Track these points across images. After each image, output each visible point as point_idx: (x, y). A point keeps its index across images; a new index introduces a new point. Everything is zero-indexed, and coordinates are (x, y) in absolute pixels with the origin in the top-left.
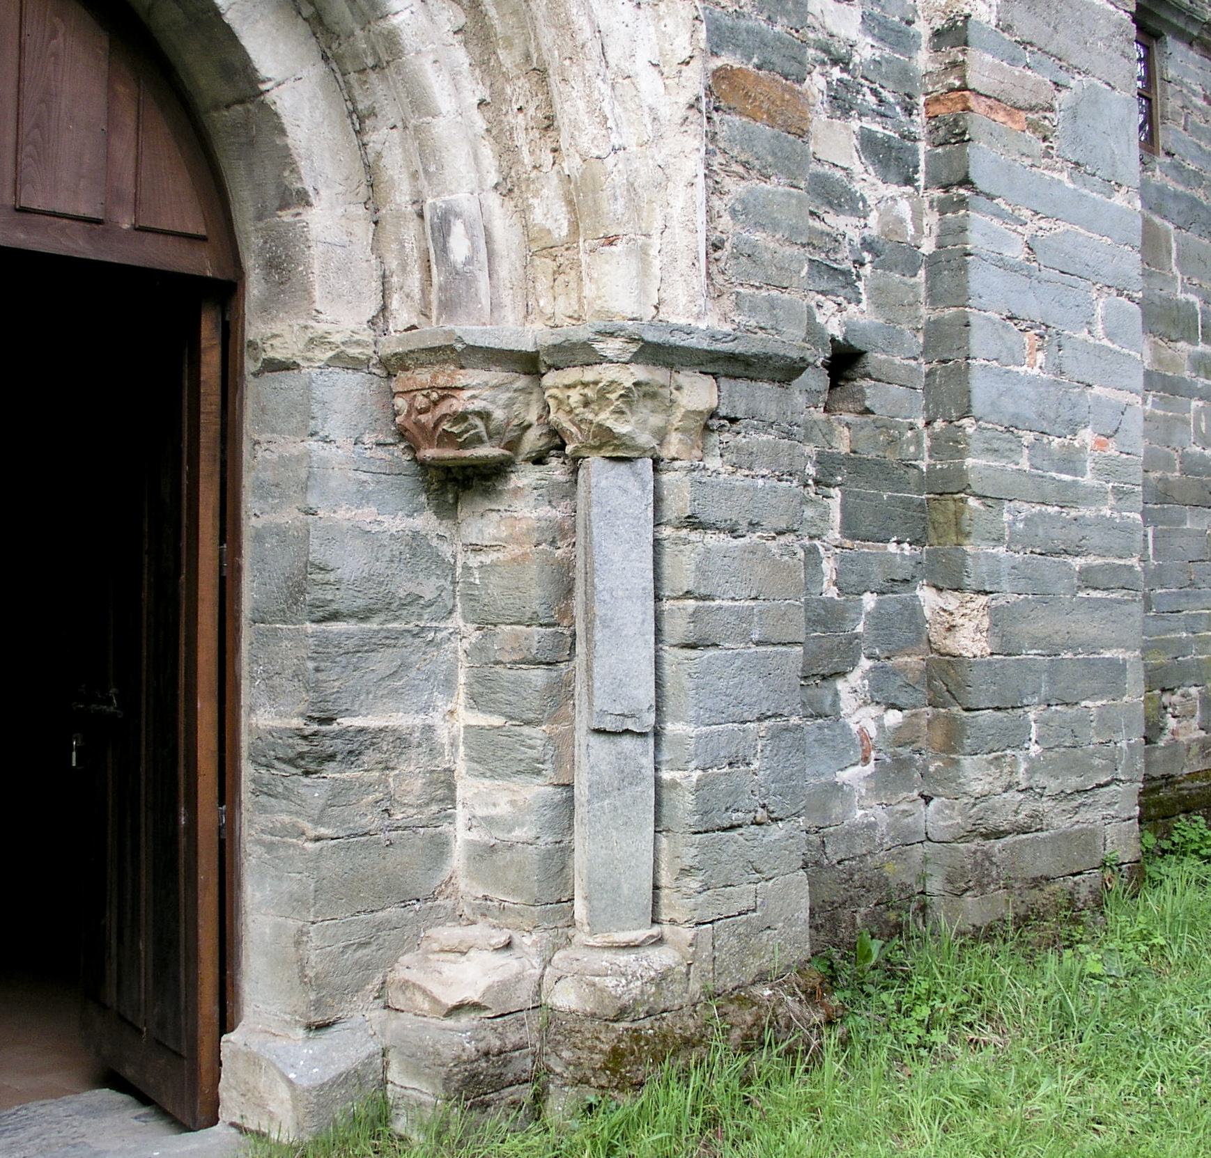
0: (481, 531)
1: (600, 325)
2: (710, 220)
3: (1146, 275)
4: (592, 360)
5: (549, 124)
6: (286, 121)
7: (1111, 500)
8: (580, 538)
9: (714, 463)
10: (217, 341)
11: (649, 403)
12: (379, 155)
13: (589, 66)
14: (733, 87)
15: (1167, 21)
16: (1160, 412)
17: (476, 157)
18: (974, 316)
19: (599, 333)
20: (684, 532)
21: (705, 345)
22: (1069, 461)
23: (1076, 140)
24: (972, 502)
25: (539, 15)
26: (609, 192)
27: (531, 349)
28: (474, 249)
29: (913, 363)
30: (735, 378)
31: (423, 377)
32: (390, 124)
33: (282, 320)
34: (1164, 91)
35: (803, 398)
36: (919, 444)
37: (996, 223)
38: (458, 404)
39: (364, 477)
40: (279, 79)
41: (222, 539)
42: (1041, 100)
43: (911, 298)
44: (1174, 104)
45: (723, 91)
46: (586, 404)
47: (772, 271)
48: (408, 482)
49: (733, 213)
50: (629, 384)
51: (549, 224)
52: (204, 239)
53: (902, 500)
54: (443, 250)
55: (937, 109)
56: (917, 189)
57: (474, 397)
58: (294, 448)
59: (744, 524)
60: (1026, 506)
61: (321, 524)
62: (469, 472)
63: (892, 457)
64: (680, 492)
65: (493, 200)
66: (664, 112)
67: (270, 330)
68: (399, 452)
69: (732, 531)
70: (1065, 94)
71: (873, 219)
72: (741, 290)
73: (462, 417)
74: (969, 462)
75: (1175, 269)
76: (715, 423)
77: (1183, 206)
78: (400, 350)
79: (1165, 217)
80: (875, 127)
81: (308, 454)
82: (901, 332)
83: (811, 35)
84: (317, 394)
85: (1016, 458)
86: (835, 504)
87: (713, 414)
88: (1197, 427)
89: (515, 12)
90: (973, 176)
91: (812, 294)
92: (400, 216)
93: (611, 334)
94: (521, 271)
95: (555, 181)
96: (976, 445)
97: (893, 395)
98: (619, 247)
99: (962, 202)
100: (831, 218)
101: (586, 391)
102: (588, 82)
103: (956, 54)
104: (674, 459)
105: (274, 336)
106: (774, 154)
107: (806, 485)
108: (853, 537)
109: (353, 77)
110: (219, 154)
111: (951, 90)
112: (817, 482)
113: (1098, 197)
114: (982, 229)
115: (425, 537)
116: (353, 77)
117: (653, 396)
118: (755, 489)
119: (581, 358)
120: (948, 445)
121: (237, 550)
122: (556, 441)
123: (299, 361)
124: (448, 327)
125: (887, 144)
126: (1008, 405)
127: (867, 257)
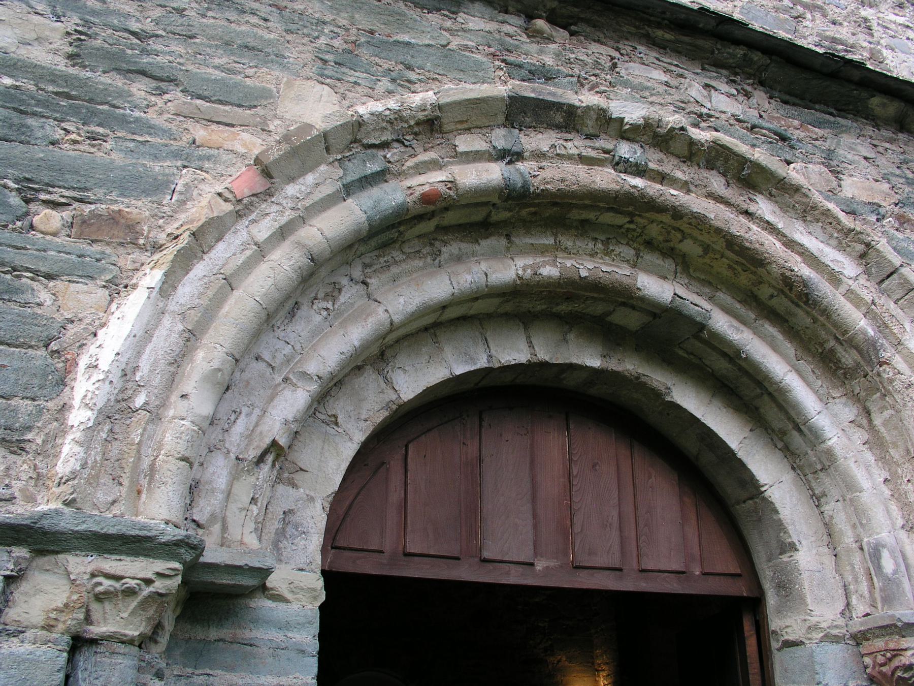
6: (778, 506)
10: (753, 632)
12: (831, 517)
17: (888, 512)
28: (897, 564)
31: (879, 644)
33: (790, 617)
40: (771, 483)
52: (739, 575)
54: (879, 567)
65: (903, 535)
67: (784, 623)
84: (817, 659)
89: (896, 428)
92: (849, 551)
105: (787, 627)
109: (810, 476)
116: (810, 476)
124: (891, 612)
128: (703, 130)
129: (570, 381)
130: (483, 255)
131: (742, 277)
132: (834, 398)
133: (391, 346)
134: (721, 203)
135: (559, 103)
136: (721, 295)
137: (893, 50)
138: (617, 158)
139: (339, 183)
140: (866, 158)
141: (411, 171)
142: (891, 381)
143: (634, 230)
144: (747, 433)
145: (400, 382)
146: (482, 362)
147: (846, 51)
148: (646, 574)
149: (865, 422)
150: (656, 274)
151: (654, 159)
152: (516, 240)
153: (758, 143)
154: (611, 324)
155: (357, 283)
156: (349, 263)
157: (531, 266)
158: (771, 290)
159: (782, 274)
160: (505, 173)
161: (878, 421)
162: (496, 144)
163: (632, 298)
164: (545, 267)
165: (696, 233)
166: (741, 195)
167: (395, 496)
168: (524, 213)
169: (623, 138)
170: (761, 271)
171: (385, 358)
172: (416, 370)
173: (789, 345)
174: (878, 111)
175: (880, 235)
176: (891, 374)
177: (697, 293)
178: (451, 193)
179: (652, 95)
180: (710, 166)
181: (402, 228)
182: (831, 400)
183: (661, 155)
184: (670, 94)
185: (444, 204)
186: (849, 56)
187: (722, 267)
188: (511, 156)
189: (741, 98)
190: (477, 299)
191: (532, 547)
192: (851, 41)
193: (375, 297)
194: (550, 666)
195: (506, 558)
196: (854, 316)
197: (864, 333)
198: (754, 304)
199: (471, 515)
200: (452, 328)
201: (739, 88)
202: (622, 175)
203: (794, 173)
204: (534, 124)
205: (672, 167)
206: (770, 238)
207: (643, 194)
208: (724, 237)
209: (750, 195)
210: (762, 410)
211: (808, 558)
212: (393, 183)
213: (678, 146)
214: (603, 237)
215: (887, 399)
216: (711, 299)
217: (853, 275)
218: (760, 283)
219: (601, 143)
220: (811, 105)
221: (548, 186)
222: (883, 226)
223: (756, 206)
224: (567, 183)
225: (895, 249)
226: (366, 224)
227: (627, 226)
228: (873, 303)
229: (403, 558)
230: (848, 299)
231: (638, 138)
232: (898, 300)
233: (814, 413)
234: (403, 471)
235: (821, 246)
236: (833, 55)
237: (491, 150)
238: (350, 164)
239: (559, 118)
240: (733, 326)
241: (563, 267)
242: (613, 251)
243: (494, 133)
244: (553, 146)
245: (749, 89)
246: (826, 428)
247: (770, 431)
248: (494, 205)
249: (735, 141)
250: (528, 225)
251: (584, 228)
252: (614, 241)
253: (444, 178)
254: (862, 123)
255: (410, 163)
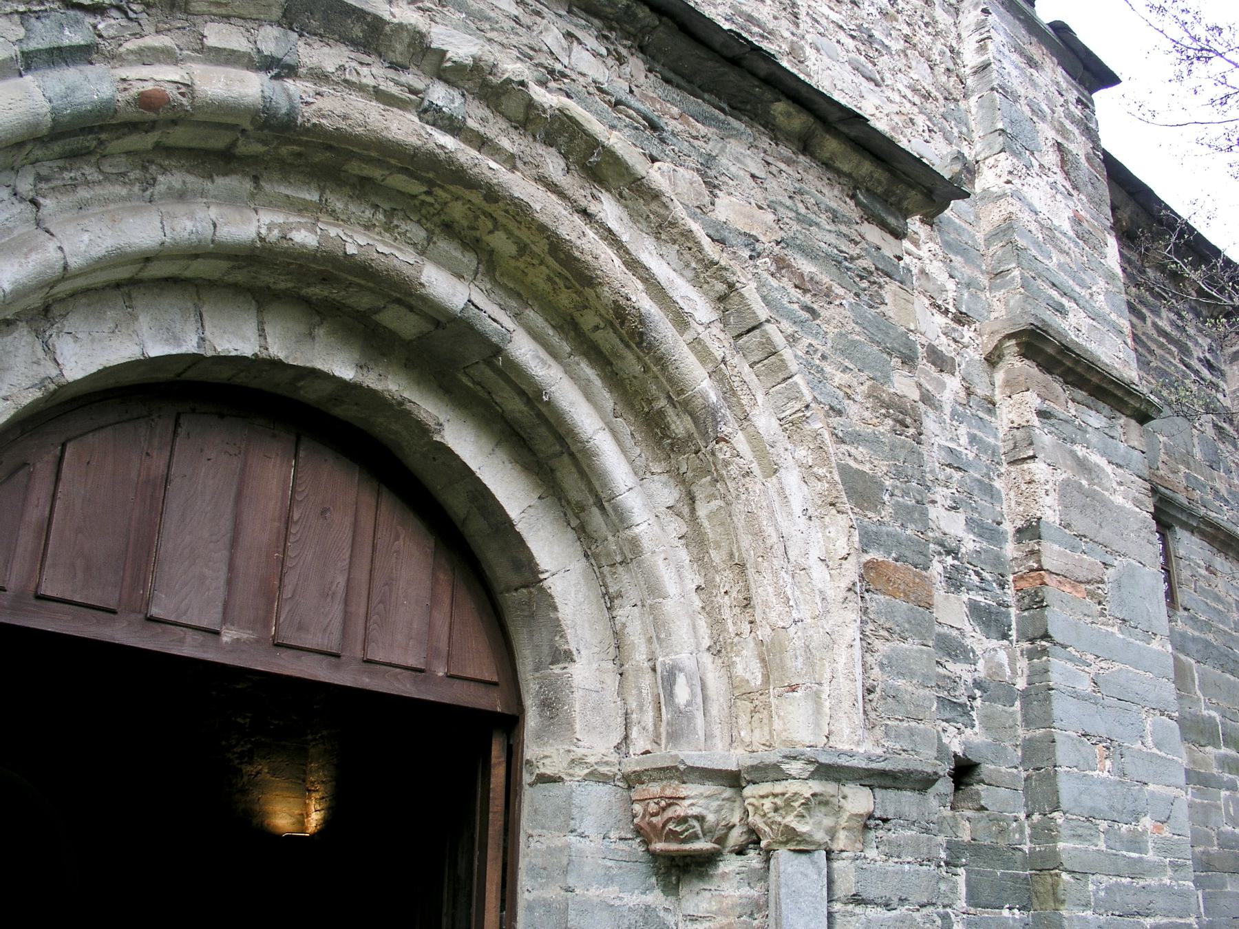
0: (697, 905)
1: (786, 751)
2: (865, 671)
3: (1180, 698)
4: (780, 776)
5: (747, 604)
6: (558, 601)
7: (1170, 872)
8: (772, 911)
9: (872, 853)
10: (503, 759)
11: (823, 809)
12: (624, 625)
13: (775, 562)
14: (879, 575)
15: (1174, 517)
16: (1198, 801)
17: (694, 627)
18: (1058, 735)
19: (785, 757)
20: (850, 907)
21: (863, 765)
22: (1136, 842)
23: (1122, 603)
24: (1065, 876)
25: (740, 526)
26: (791, 653)
27: (734, 768)
28: (693, 694)
29: (1015, 771)
30: (886, 788)
31: (655, 789)
32: (633, 603)
33: (551, 745)
34: (1178, 565)
35: (936, 803)
36: (1022, 832)
37: (1069, 665)
38: (680, 810)
39: (610, 863)
40: (554, 571)
41: (503, 908)
42: (1095, 576)
43: (1011, 723)
44: (1186, 574)
45: (872, 578)
46: (776, 810)
47: (911, 708)
48: (643, 868)
49: (882, 666)
50: (808, 795)
51: (747, 676)
52: (495, 684)
53: (1012, 876)
54: (671, 695)
55: (1022, 584)
56: (1011, 642)
57: (692, 805)
58: (558, 841)
59: (896, 900)
60: (1106, 878)
61: (577, 899)
62: (688, 860)
63: (1002, 843)
64: (847, 877)
65: (707, 658)
66: (830, 594)
67: (541, 751)
68: (636, 846)
69: (887, 905)
70: (1111, 571)
71: (981, 665)
72: (888, 722)
73: (683, 820)
74: (1061, 845)
75: (1198, 692)
76: (872, 823)
77: (1199, 647)
78: (638, 769)
79: (1188, 655)
80: (979, 598)
81: (569, 846)
82: (1005, 748)
83: (931, 534)
84: (576, 801)
85: (1095, 841)
86: (961, 880)
87: (871, 816)
88: (1227, 812)
89: (722, 524)
90: (1051, 632)
91: (938, 722)
92: (638, 670)
93: (795, 758)
94: (727, 710)
95: (752, 644)
96: (1065, 832)
97: (1000, 795)
98: (799, 694)
99: (1044, 651)
100: (950, 665)
101: (776, 800)
102: (775, 573)
103: (1033, 545)
104: (842, 851)
105: (546, 757)
106: (909, 622)
107: (939, 866)
108: (976, 906)
109: (606, 569)
110: (509, 622)
111: (1032, 570)
112: (947, 864)
113: (1141, 643)
114: (1059, 669)
115: (654, 909)
116: (606, 569)
117: (826, 803)
118: (903, 872)
119: (772, 775)
120: (1045, 833)
121: (513, 916)
122: (754, 837)
123: (563, 776)
124: (674, 752)
125: (988, 611)
126: (1087, 801)
127: (978, 693)
128: (550, 91)
129: (310, 393)
130: (215, 197)
131: (563, 296)
132: (653, 474)
133: (62, 300)
134: (554, 192)
135: (362, 10)
136: (530, 314)
137: (818, 50)
138: (426, 103)
139: (16, 48)
140: (753, 176)
141: (131, 57)
142: (726, 464)
143: (432, 205)
144: (534, 500)
145: (65, 353)
146: (189, 346)
147: (762, 36)
148: (372, 666)
149: (686, 510)
150: (449, 269)
151: (475, 115)
152: (267, 187)
153: (620, 125)
154: (377, 324)
155: (22, 200)
156: (15, 170)
157: (280, 225)
158: (597, 320)
159: (615, 302)
160: (266, 89)
161: (702, 511)
162: (262, 47)
163: (411, 295)
164: (299, 230)
165: (512, 225)
166: (582, 187)
167: (35, 513)
168: (284, 150)
169: (440, 78)
170: (588, 291)
171: (50, 315)
172: (93, 340)
173: (608, 396)
174: (781, 120)
175: (750, 276)
176: (728, 455)
177: (500, 305)
178: (184, 101)
179: (493, 29)
180: (549, 141)
181: (103, 136)
182: (648, 475)
183: (487, 113)
184: (517, 34)
185: (171, 115)
186: (765, 45)
187: (538, 277)
188: (280, 68)
189: (610, 61)
190: (196, 256)
191: (220, 609)
192: (771, 25)
193: (46, 225)
194: (245, 779)
195: (183, 620)
196: (696, 373)
197: (705, 398)
198: (572, 333)
199: (142, 556)
200: (156, 290)
201: (612, 47)
202: (428, 128)
203: (657, 176)
204: (321, 31)
205: (496, 130)
206: (609, 251)
207: (451, 160)
208: (548, 238)
209: (594, 191)
210: (558, 474)
211: (585, 673)
212: (100, 68)
213: (513, 105)
214: (387, 206)
215: (718, 485)
216: (517, 316)
217: (705, 320)
218: (586, 307)
219: (409, 78)
220: (699, 92)
221: (324, 121)
222: (756, 267)
223: (599, 206)
224: (349, 122)
225: (764, 298)
226: (49, 118)
227: (423, 197)
228: (724, 361)
229: (34, 602)
230: (693, 349)
231: (460, 83)
232: (756, 363)
233: (623, 488)
234: (53, 478)
235: (673, 275)
236: (739, 35)
237: (253, 54)
238: (38, 25)
239: (357, 32)
240: (538, 357)
241: (324, 236)
242: (397, 226)
243: (262, 31)
244: (342, 68)
245: (624, 52)
246: (635, 510)
247: (563, 503)
248: (243, 131)
249: (588, 115)
250: (287, 169)
251: (363, 189)
252: (401, 214)
253: (177, 78)
254: (759, 131)
255: (132, 45)
